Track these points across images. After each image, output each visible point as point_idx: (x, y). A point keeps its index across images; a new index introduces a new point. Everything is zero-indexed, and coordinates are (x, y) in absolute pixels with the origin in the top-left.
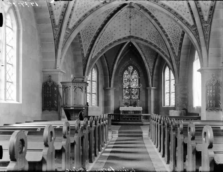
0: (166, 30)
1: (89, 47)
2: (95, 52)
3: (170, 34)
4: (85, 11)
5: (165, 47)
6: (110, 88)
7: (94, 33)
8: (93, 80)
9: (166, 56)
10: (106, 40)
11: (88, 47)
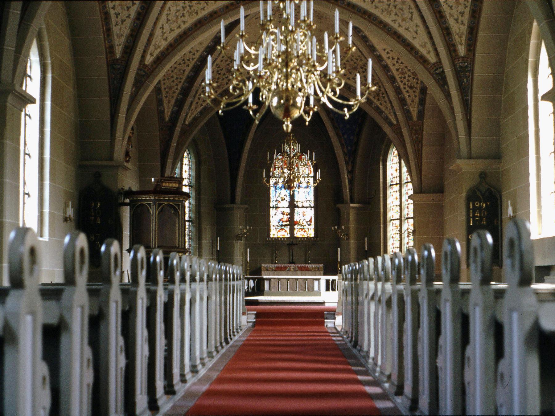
0: (384, 55)
1: (179, 94)
2: (193, 107)
3: (394, 65)
4: (182, 24)
5: (385, 95)
6: (232, 205)
7: (193, 59)
8: (399, 221)
9: (386, 119)
10: (224, 74)
11: (176, 94)
